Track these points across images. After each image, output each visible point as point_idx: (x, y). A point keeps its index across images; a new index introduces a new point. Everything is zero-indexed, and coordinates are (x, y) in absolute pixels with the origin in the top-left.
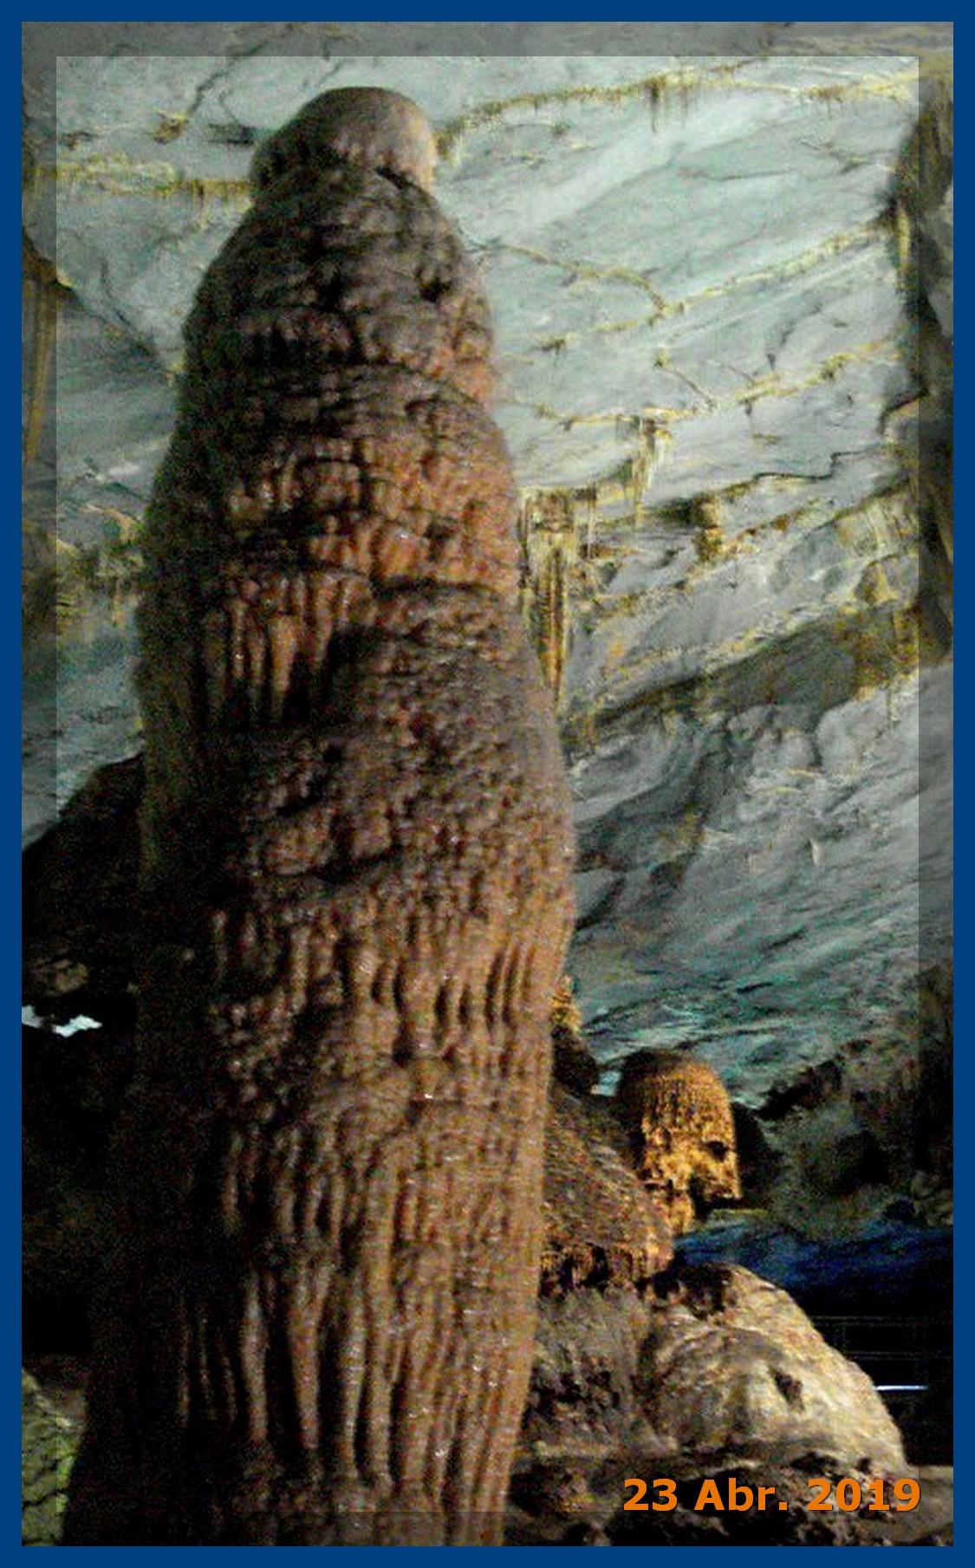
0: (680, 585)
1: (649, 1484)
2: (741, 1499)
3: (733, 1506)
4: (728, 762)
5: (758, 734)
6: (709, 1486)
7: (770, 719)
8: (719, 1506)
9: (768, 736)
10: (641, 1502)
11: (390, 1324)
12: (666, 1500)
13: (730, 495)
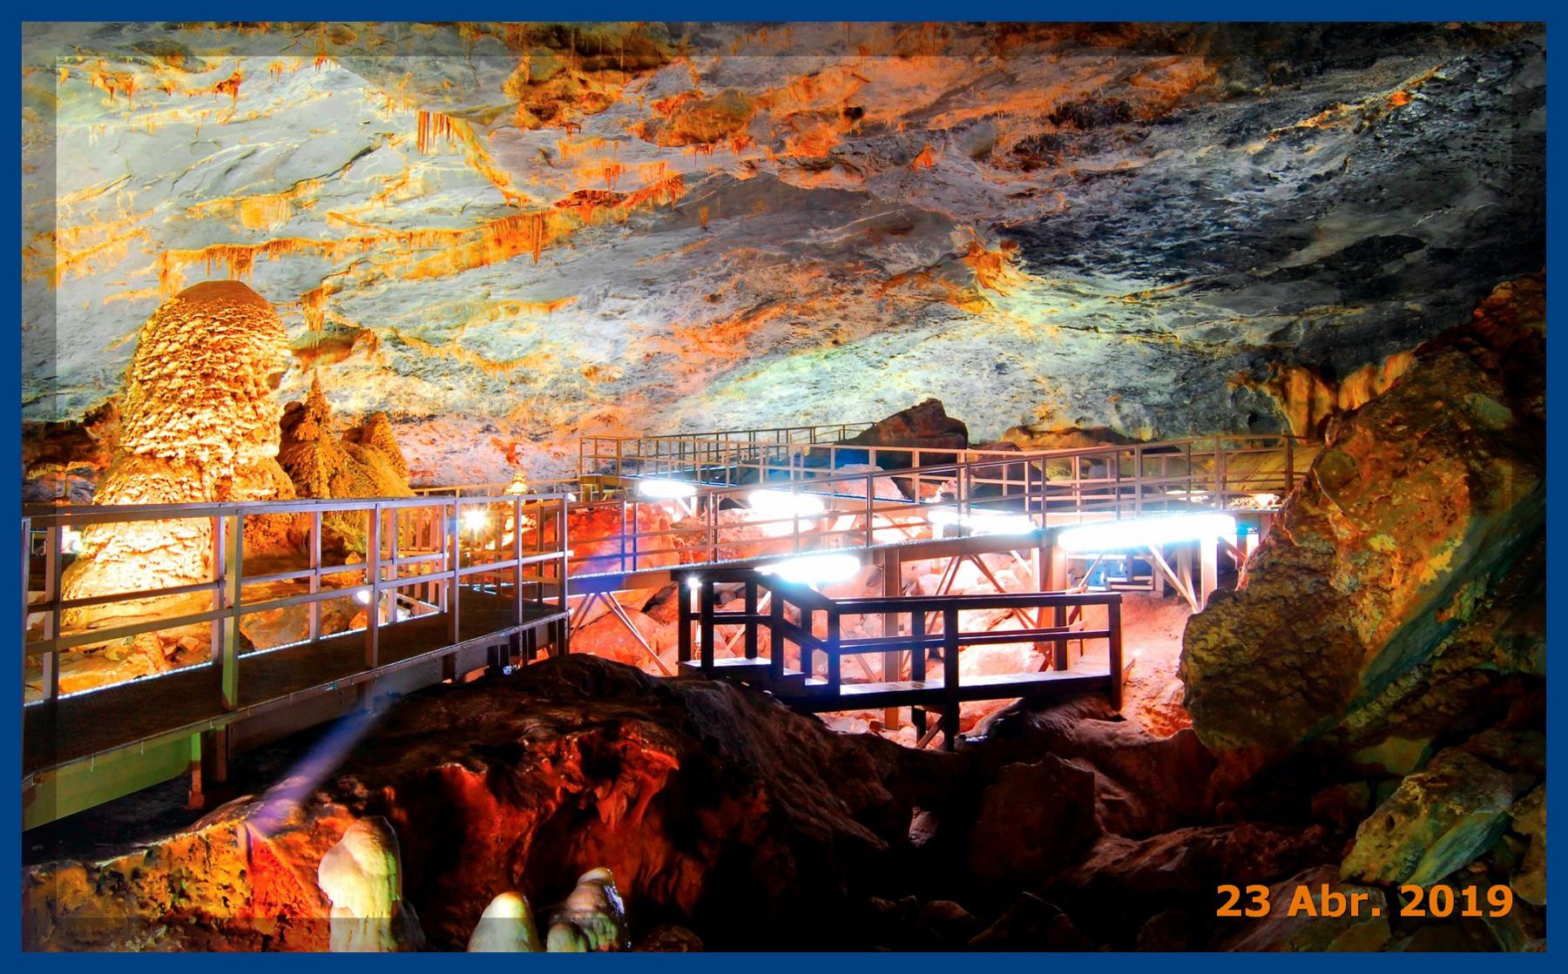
2: (1333, 904)
3: (1326, 912)
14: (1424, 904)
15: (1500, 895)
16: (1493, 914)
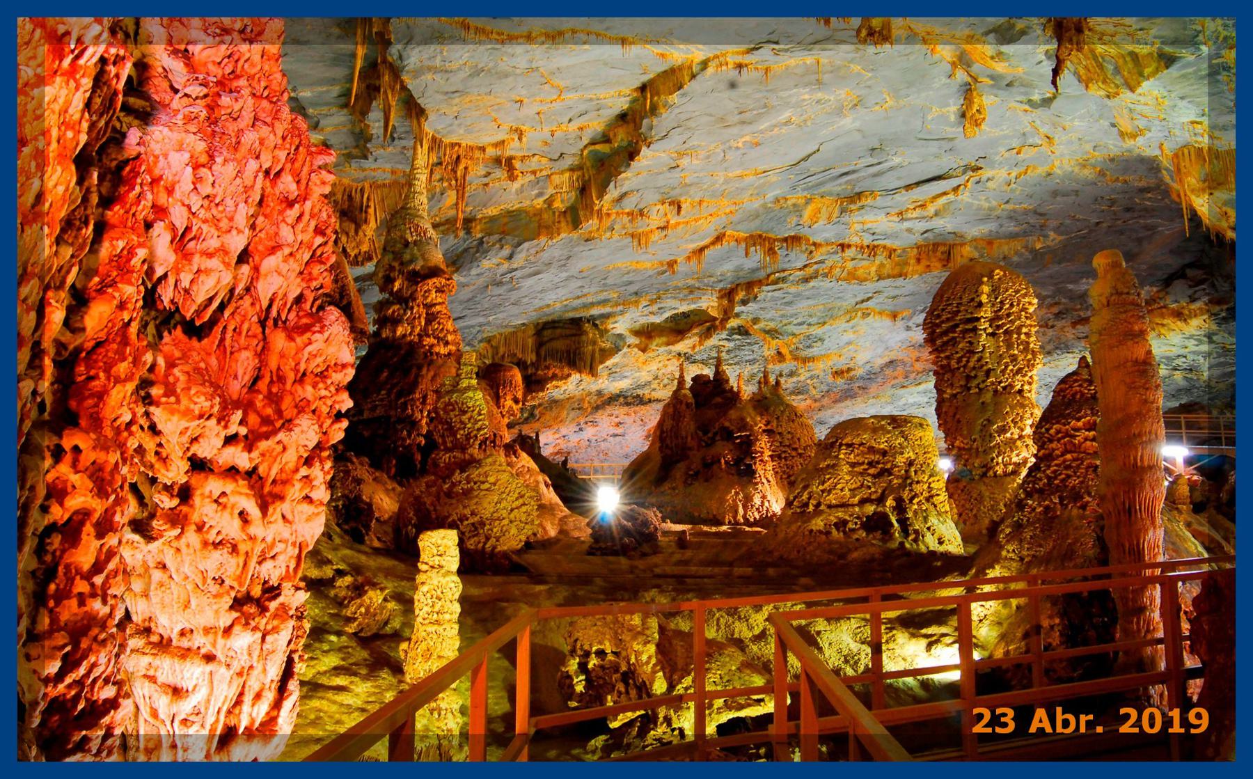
0: (486, 185)
1: (993, 712)
2: (1066, 724)
3: (1059, 729)
4: (477, 252)
5: (494, 245)
6: (1041, 713)
7: (500, 240)
8: (1049, 730)
9: (498, 246)
10: (986, 726)
11: (915, 589)
12: (1005, 725)
13: (523, 159)
14: (1138, 723)
15: (1199, 716)
16: (1193, 731)
